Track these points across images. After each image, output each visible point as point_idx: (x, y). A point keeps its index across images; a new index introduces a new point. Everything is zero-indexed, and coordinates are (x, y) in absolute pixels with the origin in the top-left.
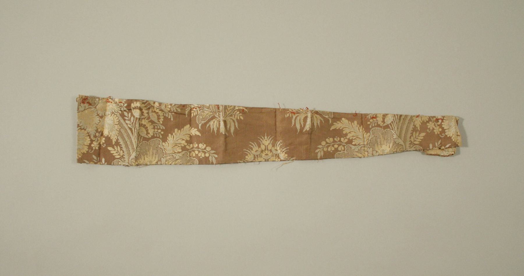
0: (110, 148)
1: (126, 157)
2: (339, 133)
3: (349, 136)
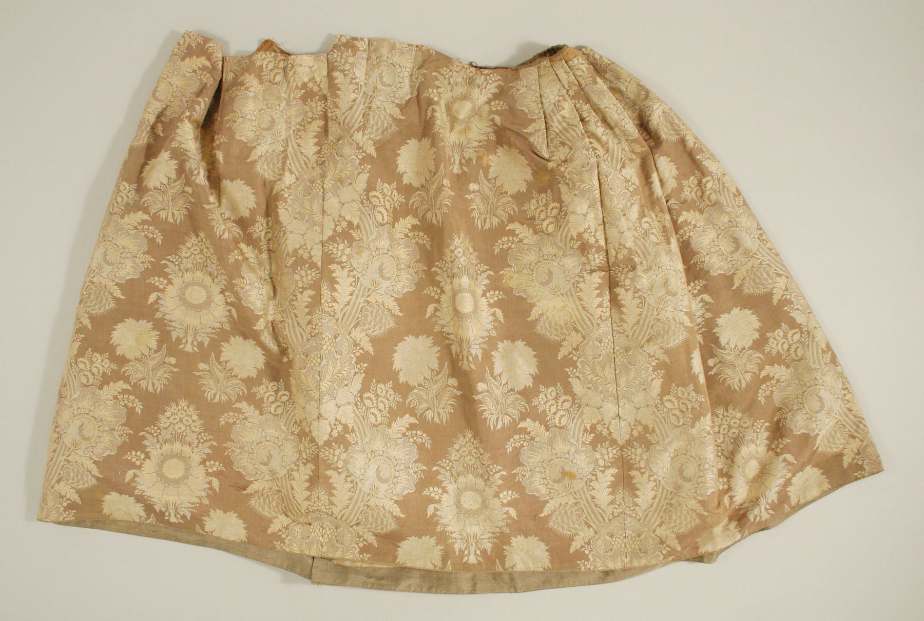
0: (347, 435)
1: (365, 238)
2: (239, 411)
3: (532, 434)
